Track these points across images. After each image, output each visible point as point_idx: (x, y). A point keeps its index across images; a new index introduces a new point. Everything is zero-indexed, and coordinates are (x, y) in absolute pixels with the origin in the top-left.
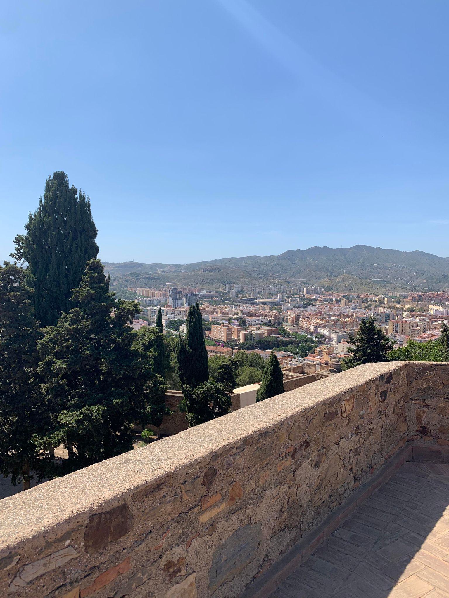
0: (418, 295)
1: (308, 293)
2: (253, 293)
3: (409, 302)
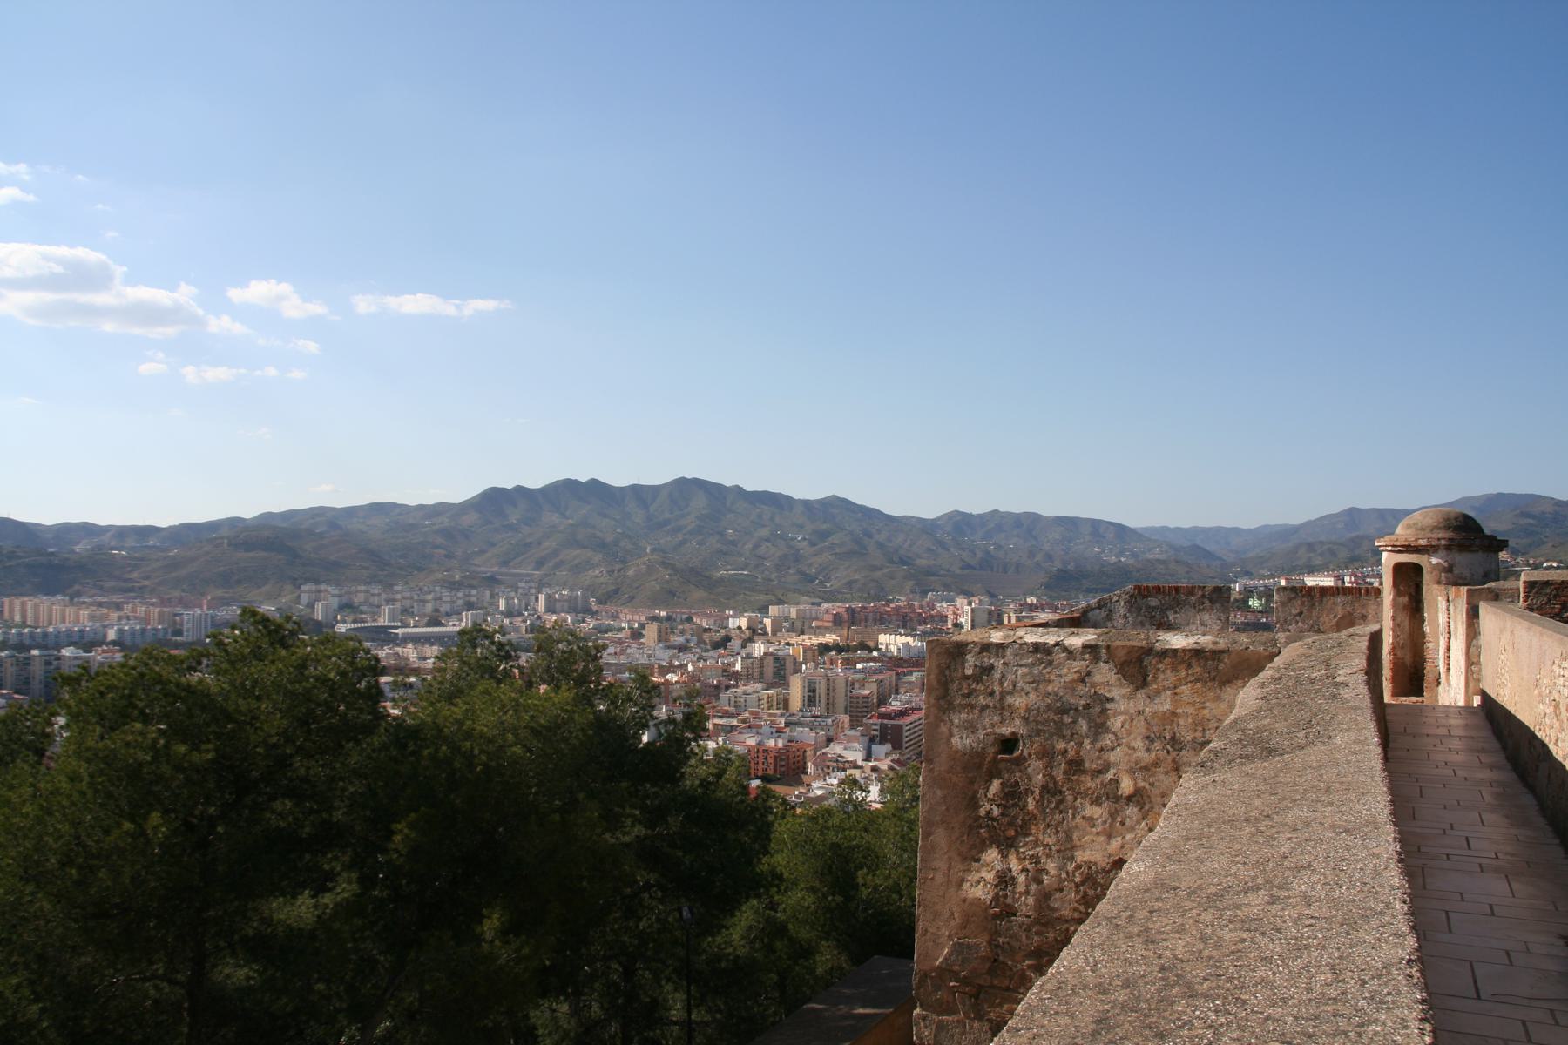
0: (848, 609)
1: (550, 609)
2: (386, 609)
3: (826, 628)
